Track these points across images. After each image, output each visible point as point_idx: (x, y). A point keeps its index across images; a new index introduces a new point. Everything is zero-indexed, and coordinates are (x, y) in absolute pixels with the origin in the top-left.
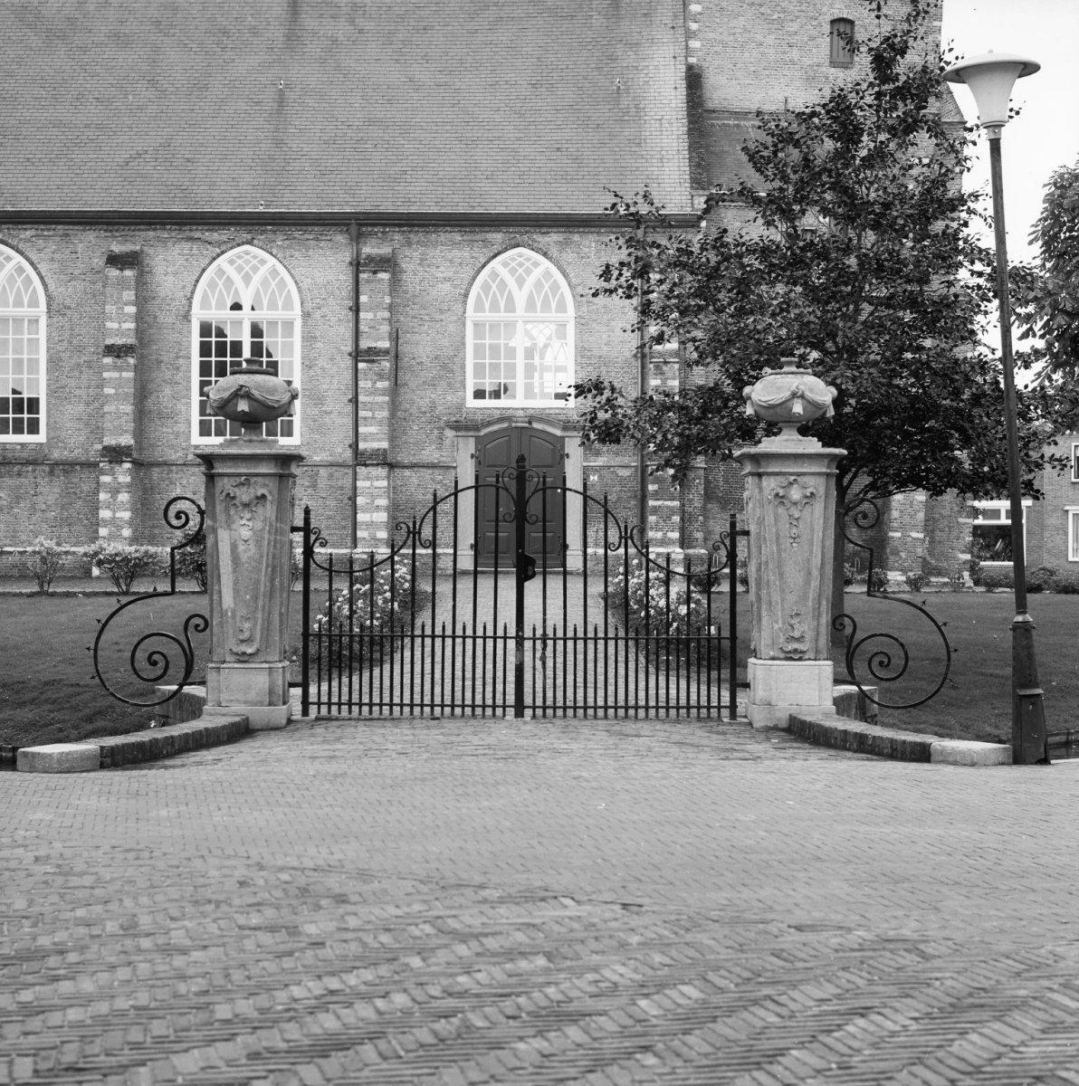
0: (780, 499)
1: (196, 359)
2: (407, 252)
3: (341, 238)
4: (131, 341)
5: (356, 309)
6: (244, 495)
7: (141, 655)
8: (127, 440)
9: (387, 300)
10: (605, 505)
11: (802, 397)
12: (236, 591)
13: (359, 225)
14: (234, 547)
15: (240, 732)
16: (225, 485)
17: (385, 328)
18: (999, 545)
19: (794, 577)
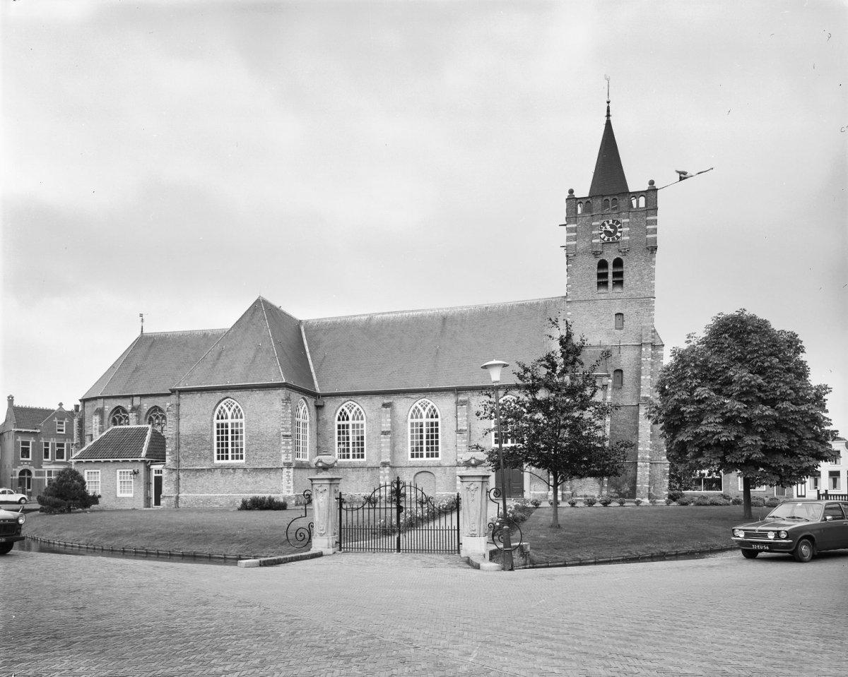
0: (468, 488)
1: (409, 434)
2: (473, 398)
3: (452, 395)
4: (389, 429)
5: (457, 417)
6: (320, 489)
7: (298, 535)
8: (388, 460)
9: (466, 414)
10: (422, 491)
11: (474, 458)
12: (319, 516)
13: (458, 391)
14: (318, 504)
15: (320, 555)
16: (315, 486)
17: (465, 423)
18: (714, 485)
19: (473, 512)
